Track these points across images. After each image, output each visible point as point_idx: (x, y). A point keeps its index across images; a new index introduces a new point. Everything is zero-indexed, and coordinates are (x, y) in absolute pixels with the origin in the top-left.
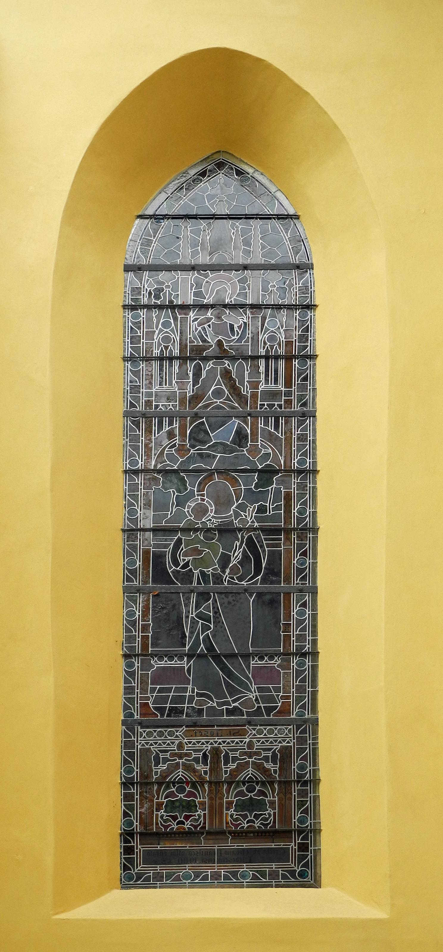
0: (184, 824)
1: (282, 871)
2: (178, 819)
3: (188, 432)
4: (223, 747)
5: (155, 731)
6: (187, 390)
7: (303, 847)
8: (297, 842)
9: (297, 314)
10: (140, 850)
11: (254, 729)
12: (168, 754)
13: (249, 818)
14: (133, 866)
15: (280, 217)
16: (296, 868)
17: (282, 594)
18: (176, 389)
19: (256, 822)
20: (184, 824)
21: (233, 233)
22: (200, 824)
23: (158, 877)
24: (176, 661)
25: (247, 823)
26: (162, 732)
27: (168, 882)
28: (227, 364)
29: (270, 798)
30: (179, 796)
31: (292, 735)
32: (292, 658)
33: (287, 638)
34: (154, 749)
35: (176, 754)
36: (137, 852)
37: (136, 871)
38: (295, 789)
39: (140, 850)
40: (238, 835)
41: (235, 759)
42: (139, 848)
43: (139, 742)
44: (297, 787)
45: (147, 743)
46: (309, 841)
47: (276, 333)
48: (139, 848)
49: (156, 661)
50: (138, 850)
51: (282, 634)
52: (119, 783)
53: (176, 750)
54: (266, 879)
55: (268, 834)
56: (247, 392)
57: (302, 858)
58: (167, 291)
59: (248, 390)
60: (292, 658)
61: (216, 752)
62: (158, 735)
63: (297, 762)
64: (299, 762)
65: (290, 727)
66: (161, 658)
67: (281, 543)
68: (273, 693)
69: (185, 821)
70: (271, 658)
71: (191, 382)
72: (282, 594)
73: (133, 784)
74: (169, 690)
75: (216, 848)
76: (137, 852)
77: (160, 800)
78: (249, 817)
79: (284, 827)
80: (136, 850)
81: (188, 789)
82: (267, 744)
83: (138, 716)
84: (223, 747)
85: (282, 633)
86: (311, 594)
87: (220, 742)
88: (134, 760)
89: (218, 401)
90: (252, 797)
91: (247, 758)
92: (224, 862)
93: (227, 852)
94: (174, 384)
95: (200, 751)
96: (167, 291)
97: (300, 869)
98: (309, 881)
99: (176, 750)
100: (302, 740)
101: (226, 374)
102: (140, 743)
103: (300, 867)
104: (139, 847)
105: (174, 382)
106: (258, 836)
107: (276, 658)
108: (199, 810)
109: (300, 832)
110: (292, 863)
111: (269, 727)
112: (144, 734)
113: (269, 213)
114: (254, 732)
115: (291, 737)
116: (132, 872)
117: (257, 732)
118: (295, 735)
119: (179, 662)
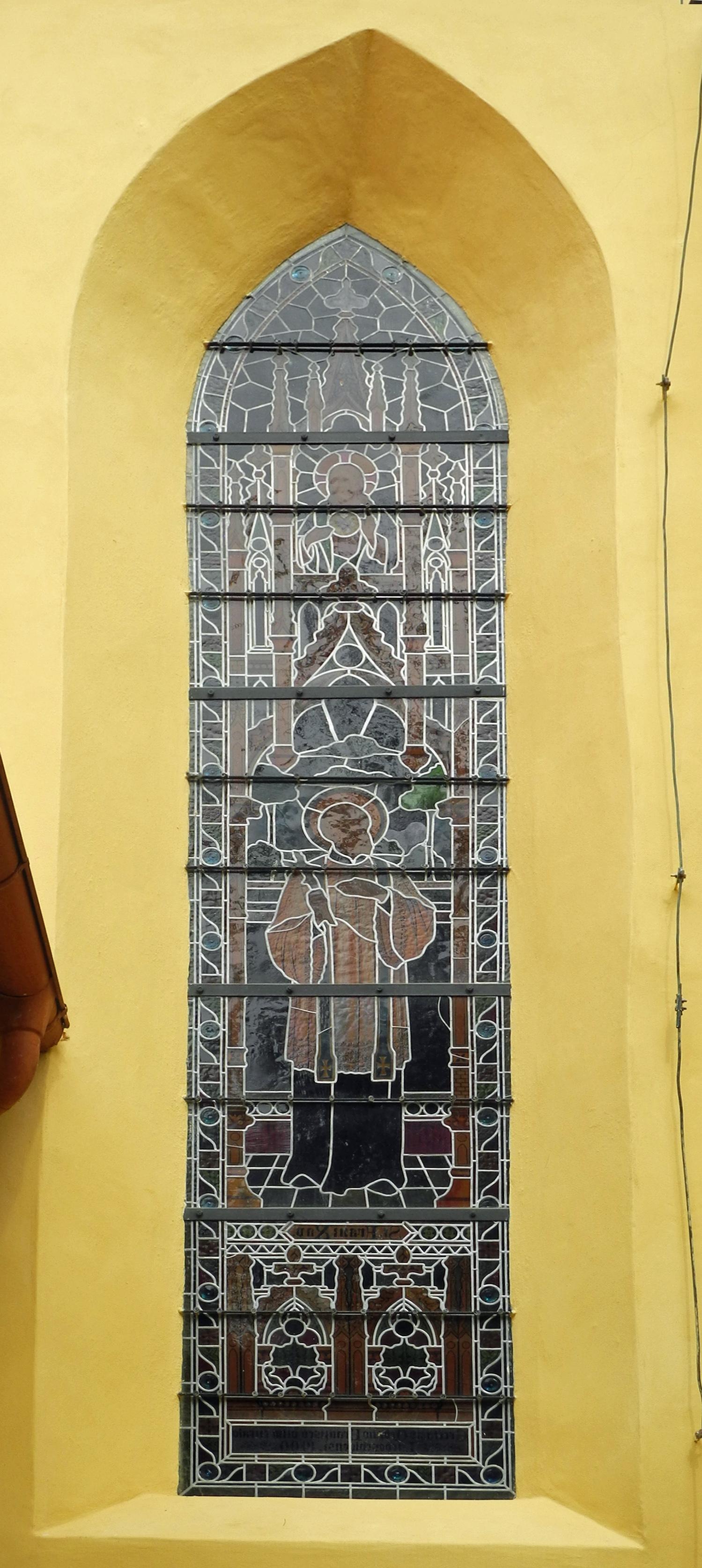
0: (411, 1386)
1: (459, 1468)
2: (290, 1375)
3: (293, 725)
4: (252, 1255)
5: (237, 1227)
6: (292, 651)
7: (492, 1430)
8: (481, 1420)
9: (377, 519)
10: (228, 1426)
11: (417, 1228)
12: (273, 1266)
13: (402, 1377)
14: (216, 1452)
15: (456, 347)
16: (480, 1464)
17: (450, 999)
18: (272, 650)
19: (415, 1385)
20: (411, 1386)
21: (370, 380)
22: (432, 1387)
23: (256, 1472)
24: (423, 1113)
25: (398, 1386)
26: (453, 1230)
27: (272, 1482)
28: (364, 607)
29: (433, 1344)
30: (290, 1338)
31: (471, 1241)
32: (470, 1109)
33: (462, 1077)
34: (255, 1257)
35: (285, 1266)
36: (223, 1431)
37: (221, 1461)
38: (478, 1330)
39: (228, 1426)
40: (389, 1406)
41: (272, 1279)
42: (227, 1423)
43: (226, 1243)
44: (481, 1327)
45: (241, 1247)
46: (501, 1418)
47: (264, 557)
48: (227, 1423)
49: (256, 1113)
50: (225, 1428)
51: (452, 1068)
52: (181, 1313)
53: (287, 1259)
54: (431, 1482)
55: (420, 1407)
56: (402, 656)
57: (489, 1448)
58: (259, 481)
59: (403, 651)
60: (470, 1109)
61: (349, 1264)
62: (262, 1233)
63: (480, 1286)
64: (483, 1286)
65: (466, 1226)
66: (265, 1106)
67: (449, 913)
68: (423, 1168)
69: (413, 1381)
70: (432, 1108)
71: (299, 639)
72: (450, 999)
73: (215, 1315)
74: (269, 1161)
75: (350, 1426)
76: (223, 1431)
77: (374, 1345)
78: (292, 1374)
79: (348, 1392)
80: (221, 1428)
81: (306, 1327)
82: (423, 1253)
83: (225, 1204)
84: (252, 1255)
85: (451, 1065)
86: (229, 1001)
87: (278, 1248)
88: (216, 1275)
89: (349, 669)
90: (406, 1345)
91: (398, 1275)
92: (364, 1450)
93: (372, 1433)
94: (268, 642)
95: (429, 1263)
96: (259, 481)
97: (487, 1466)
98: (194, 1480)
99: (287, 1259)
100: (488, 1250)
101: (363, 624)
102: (228, 1246)
103: (487, 1462)
104: (227, 1420)
105: (267, 637)
106: (276, 1406)
107: (440, 1109)
108: (320, 1362)
109: (486, 1402)
110: (473, 1455)
111: (445, 1225)
112: (237, 1232)
113: (436, 341)
114: (416, 1233)
115: (469, 1243)
116: (214, 1463)
117: (274, 1232)
118: (477, 1240)
119: (428, 1115)
